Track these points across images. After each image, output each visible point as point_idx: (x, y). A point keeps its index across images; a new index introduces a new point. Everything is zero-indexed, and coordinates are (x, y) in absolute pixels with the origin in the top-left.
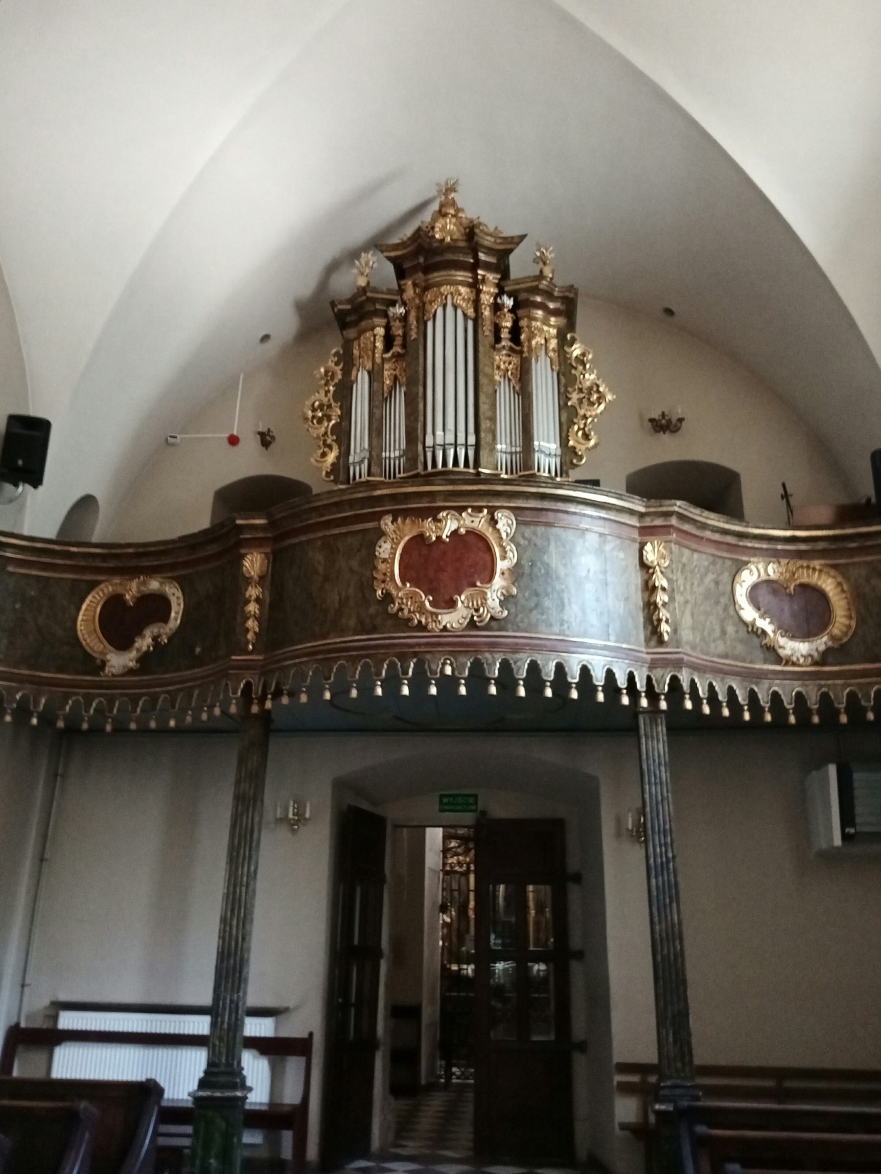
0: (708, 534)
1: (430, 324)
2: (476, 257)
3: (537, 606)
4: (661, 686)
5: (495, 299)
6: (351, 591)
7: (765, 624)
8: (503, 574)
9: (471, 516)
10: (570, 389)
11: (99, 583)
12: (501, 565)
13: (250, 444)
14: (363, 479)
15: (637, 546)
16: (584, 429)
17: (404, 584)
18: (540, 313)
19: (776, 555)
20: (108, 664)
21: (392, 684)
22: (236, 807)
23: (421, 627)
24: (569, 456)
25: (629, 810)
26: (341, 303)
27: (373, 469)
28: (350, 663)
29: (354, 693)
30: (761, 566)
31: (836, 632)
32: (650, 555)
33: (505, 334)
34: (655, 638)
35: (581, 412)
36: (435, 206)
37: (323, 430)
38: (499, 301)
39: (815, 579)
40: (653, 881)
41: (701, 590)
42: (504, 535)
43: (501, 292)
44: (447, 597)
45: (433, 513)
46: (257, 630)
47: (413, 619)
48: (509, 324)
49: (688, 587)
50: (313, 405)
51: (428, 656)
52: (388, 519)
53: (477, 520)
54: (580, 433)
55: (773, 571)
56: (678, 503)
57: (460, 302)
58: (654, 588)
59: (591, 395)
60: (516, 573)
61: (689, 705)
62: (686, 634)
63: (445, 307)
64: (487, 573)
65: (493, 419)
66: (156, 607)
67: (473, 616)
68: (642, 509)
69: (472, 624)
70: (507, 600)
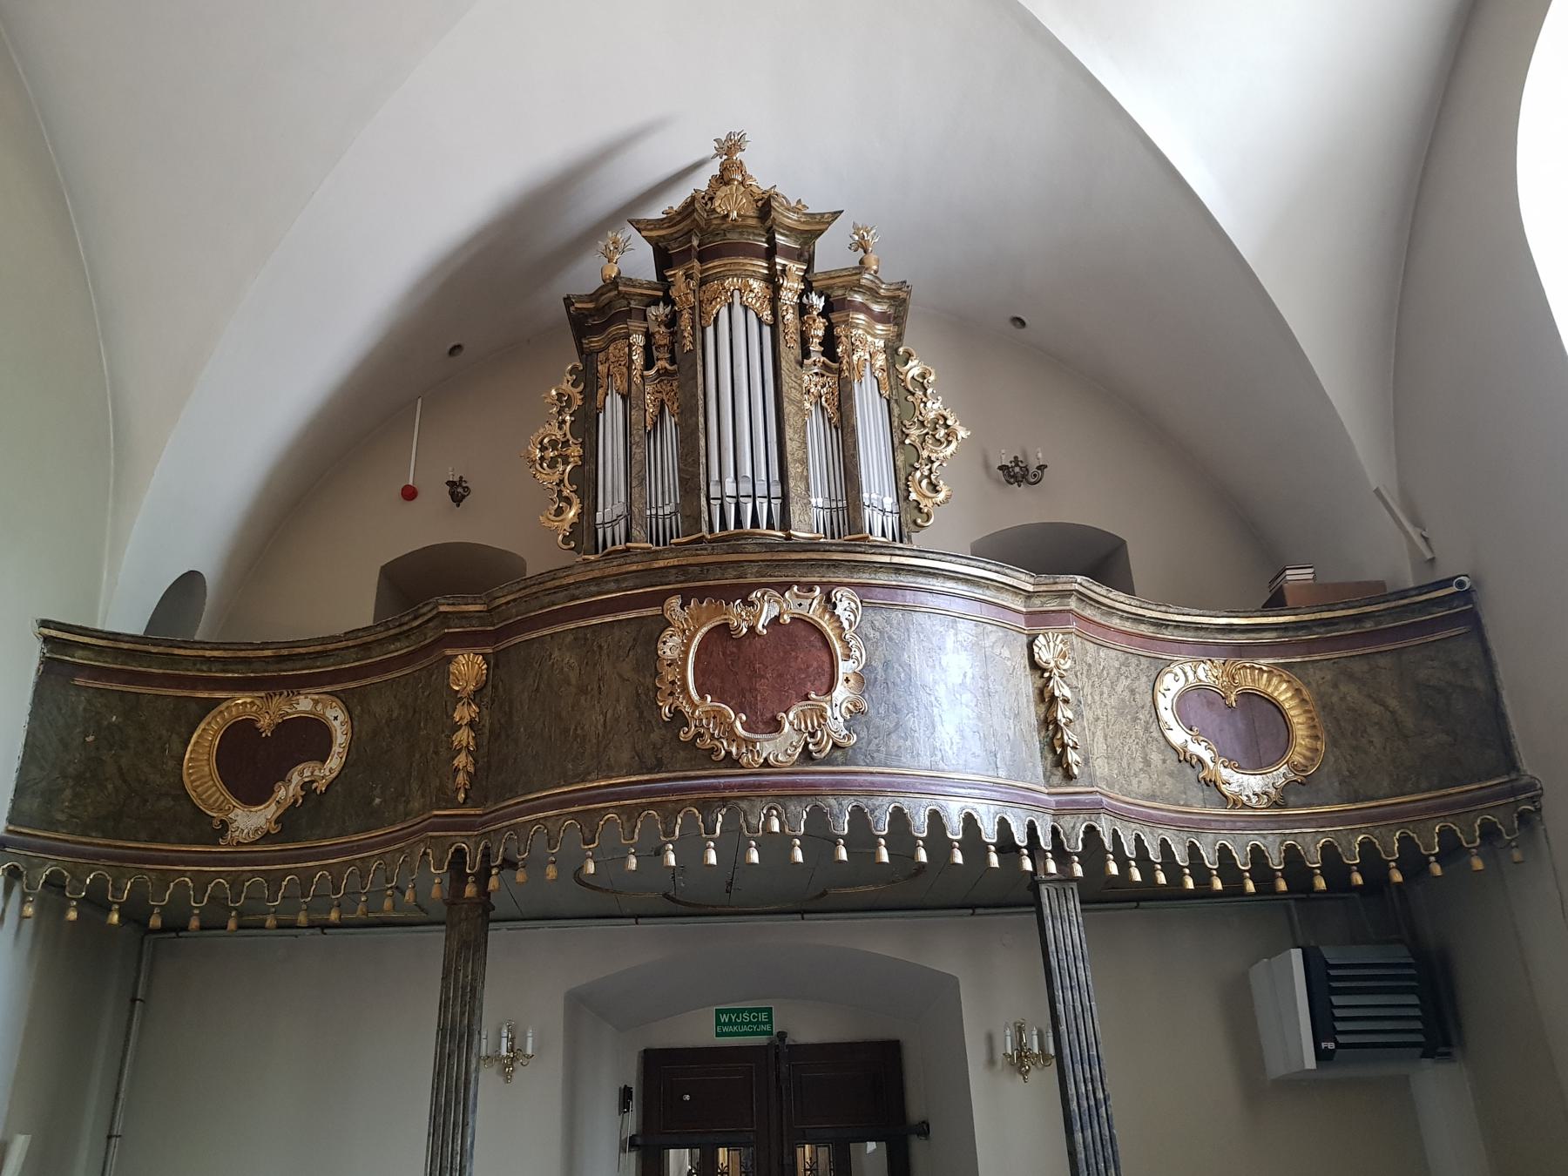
0: (1116, 622)
1: (710, 331)
2: (771, 241)
3: (897, 726)
4: (1072, 842)
5: (800, 297)
6: (621, 708)
7: (1200, 750)
8: (847, 680)
9: (798, 596)
10: (907, 423)
11: (219, 701)
12: (844, 668)
13: (435, 495)
14: (619, 547)
15: (1025, 639)
16: (929, 477)
17: (703, 698)
18: (861, 318)
19: (1205, 651)
20: (232, 827)
21: (691, 849)
22: (441, 1044)
23: (731, 761)
24: (911, 516)
25: (1007, 1026)
26: (581, 298)
27: (635, 533)
28: (624, 817)
29: (633, 863)
30: (1187, 668)
31: (1297, 759)
32: (1044, 655)
33: (815, 347)
34: (1059, 772)
35: (925, 454)
36: (714, 169)
37: (556, 477)
38: (805, 300)
39: (1263, 684)
40: (1078, 1136)
41: (1113, 701)
42: (846, 625)
43: (808, 288)
44: (769, 715)
45: (742, 593)
46: (471, 769)
47: (719, 750)
48: (821, 333)
49: (1097, 698)
50: (541, 442)
51: (744, 805)
52: (675, 602)
53: (806, 603)
54: (925, 482)
55: (1206, 673)
56: (1079, 579)
57: (750, 299)
58: (1053, 698)
59: (938, 430)
60: (863, 680)
61: (1113, 869)
62: (1101, 767)
63: (730, 307)
64: (825, 679)
65: (804, 462)
66: (308, 738)
67: (807, 744)
68: (1030, 588)
69: (807, 755)
70: (856, 715)
